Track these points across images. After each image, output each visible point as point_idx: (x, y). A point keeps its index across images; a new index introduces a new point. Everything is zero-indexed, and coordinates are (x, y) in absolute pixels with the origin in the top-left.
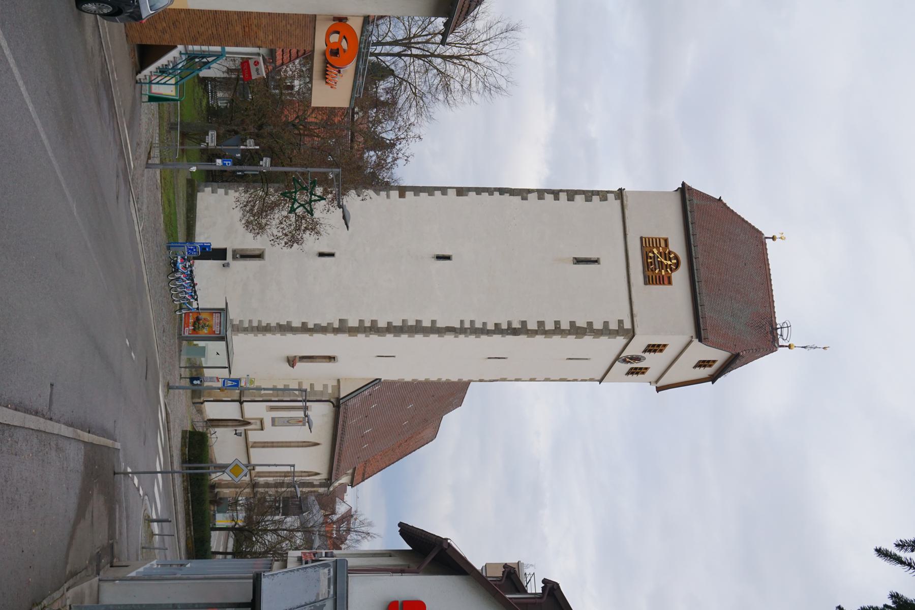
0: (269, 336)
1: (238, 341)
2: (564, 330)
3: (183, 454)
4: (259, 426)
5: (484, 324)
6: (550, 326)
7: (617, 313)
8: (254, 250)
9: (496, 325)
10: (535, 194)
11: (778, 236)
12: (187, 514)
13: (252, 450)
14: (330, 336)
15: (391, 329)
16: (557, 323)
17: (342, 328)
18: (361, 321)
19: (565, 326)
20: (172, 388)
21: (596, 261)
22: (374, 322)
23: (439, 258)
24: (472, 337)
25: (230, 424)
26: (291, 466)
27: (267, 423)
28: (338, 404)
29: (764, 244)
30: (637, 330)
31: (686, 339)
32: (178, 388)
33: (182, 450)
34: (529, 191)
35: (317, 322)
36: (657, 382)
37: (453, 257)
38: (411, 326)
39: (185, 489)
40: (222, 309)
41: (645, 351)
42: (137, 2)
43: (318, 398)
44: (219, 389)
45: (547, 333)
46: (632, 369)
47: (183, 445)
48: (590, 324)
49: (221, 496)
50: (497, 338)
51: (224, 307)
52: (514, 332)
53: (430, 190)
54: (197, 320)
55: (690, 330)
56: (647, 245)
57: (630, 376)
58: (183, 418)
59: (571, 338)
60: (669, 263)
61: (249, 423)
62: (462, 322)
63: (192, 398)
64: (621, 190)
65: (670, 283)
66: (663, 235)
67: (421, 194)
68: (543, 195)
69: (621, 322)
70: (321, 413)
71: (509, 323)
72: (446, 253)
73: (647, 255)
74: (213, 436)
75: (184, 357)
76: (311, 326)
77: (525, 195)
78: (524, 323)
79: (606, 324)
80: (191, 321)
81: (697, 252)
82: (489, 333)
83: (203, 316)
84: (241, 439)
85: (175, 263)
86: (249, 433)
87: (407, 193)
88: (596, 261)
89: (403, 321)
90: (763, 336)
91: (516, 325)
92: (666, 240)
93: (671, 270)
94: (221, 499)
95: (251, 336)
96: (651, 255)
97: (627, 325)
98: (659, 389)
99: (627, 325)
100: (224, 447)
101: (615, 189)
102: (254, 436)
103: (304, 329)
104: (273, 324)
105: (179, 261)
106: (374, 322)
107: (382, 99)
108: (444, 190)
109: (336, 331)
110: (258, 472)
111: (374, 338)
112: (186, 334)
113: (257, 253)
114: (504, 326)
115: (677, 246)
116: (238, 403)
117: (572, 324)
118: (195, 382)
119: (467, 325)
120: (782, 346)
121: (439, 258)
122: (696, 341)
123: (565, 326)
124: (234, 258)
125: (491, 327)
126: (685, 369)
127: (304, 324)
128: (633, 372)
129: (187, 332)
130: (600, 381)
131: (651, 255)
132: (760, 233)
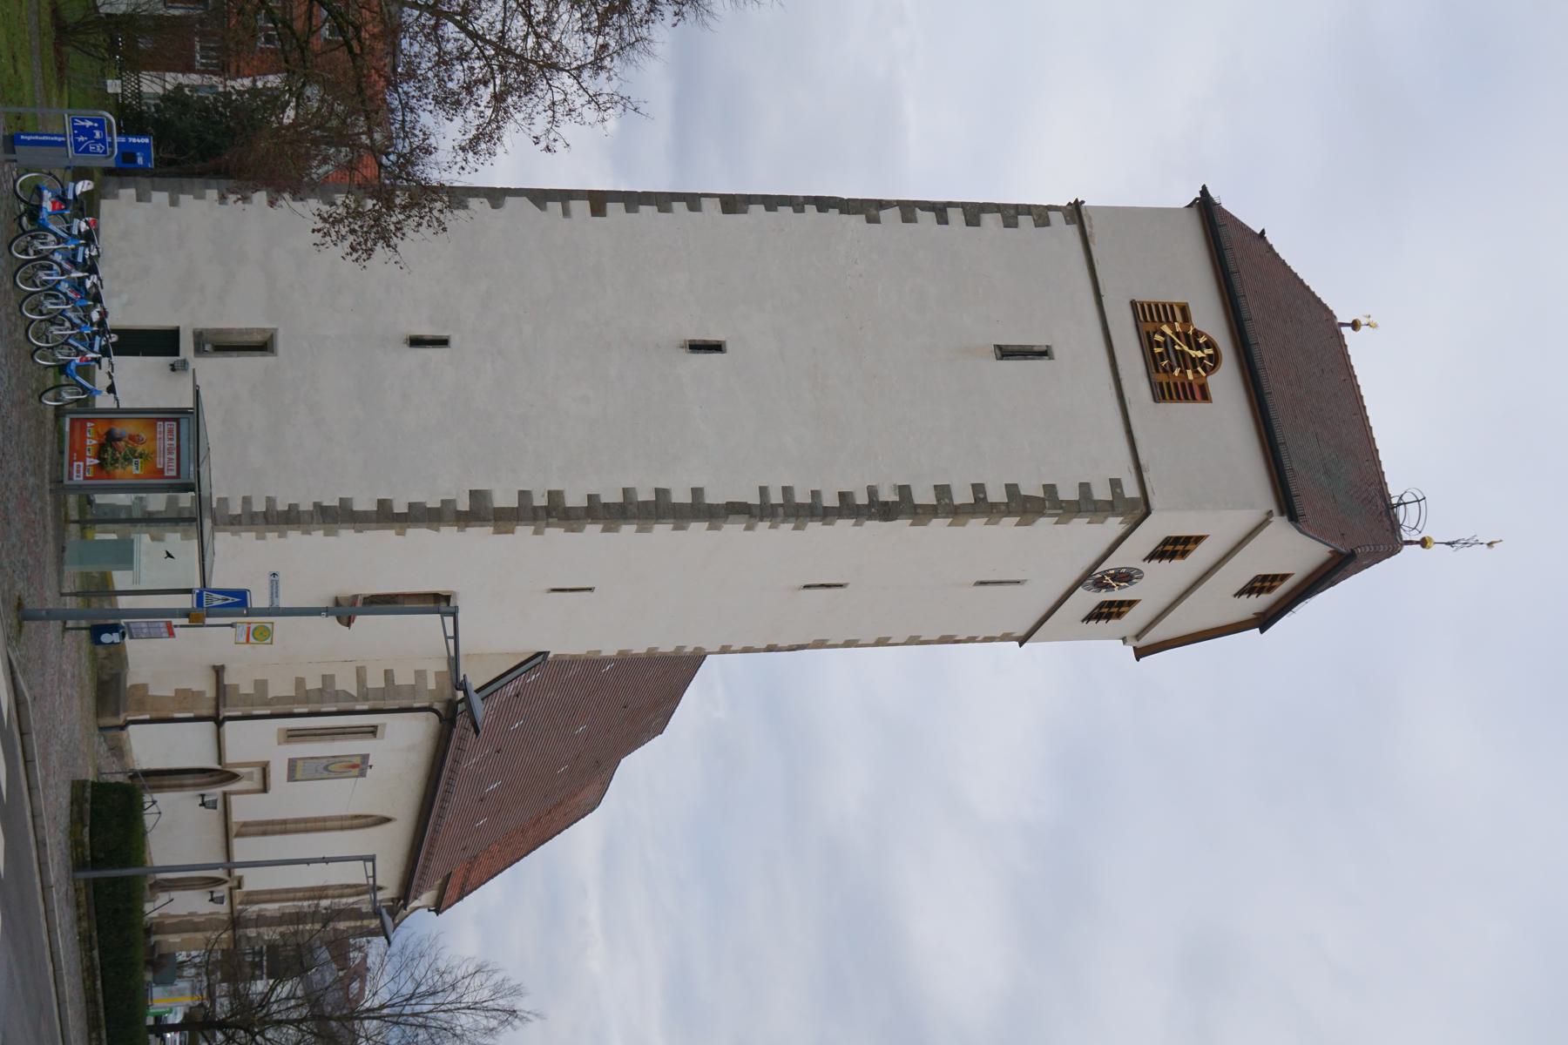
0: (294, 536)
2: (994, 505)
3: (76, 844)
4: (256, 784)
5: (816, 494)
6: (963, 496)
7: (1105, 465)
8: (249, 331)
9: (842, 496)
10: (896, 211)
11: (1363, 321)
12: (90, 1000)
14: (449, 533)
16: (978, 489)
17: (479, 512)
18: (524, 495)
19: (996, 495)
20: (33, 617)
21: (1044, 353)
22: (555, 496)
23: (697, 347)
25: (189, 780)
27: (278, 773)
28: (452, 716)
30: (1154, 501)
31: (1256, 516)
32: (50, 615)
33: (72, 833)
34: (882, 205)
36: (1138, 637)
37: (729, 347)
38: (645, 503)
39: (85, 940)
40: (183, 411)
41: (1152, 556)
42: (90, 1040)
43: (405, 703)
44: (186, 614)
45: (957, 513)
46: (1102, 605)
47: (76, 820)
48: (1050, 489)
49: (165, 950)
50: (844, 525)
51: (188, 403)
52: (885, 512)
54: (109, 440)
55: (1264, 499)
56: (1147, 315)
58: (70, 752)
60: (1200, 354)
61: (234, 777)
62: (763, 491)
63: (98, 715)
64: (1077, 205)
65: (1205, 397)
66: (1177, 298)
67: (642, 208)
68: (913, 212)
69: (1115, 484)
70: (403, 743)
71: (872, 492)
72: (713, 336)
73: (1149, 337)
74: (154, 809)
75: (71, 570)
76: (400, 507)
78: (904, 491)
79: (1085, 488)
80: (91, 442)
83: (125, 429)
84: (215, 816)
85: (34, 212)
86: (234, 799)
87: (609, 205)
88: (1044, 353)
89: (625, 491)
91: (888, 495)
92: (1184, 309)
93: (1204, 369)
94: (161, 956)
95: (248, 537)
96: (1158, 338)
97: (1131, 490)
98: (1140, 653)
99: (1131, 490)
100: (175, 831)
102: (245, 808)
103: (384, 516)
104: (306, 506)
105: (48, 205)
106: (555, 496)
108: (693, 201)
109: (465, 519)
110: (249, 894)
111: (555, 534)
112: (78, 479)
113: (258, 338)
114: (862, 499)
115: (1209, 319)
116: (211, 725)
117: (1012, 489)
118: (106, 638)
119: (776, 498)
121: (697, 347)
122: (1280, 524)
123: (996, 495)
124: (199, 350)
125: (831, 500)
126: (1220, 599)
127: (384, 504)
128: (1106, 612)
129: (80, 472)
130: (1022, 641)
131: (1158, 338)
132: (1330, 314)
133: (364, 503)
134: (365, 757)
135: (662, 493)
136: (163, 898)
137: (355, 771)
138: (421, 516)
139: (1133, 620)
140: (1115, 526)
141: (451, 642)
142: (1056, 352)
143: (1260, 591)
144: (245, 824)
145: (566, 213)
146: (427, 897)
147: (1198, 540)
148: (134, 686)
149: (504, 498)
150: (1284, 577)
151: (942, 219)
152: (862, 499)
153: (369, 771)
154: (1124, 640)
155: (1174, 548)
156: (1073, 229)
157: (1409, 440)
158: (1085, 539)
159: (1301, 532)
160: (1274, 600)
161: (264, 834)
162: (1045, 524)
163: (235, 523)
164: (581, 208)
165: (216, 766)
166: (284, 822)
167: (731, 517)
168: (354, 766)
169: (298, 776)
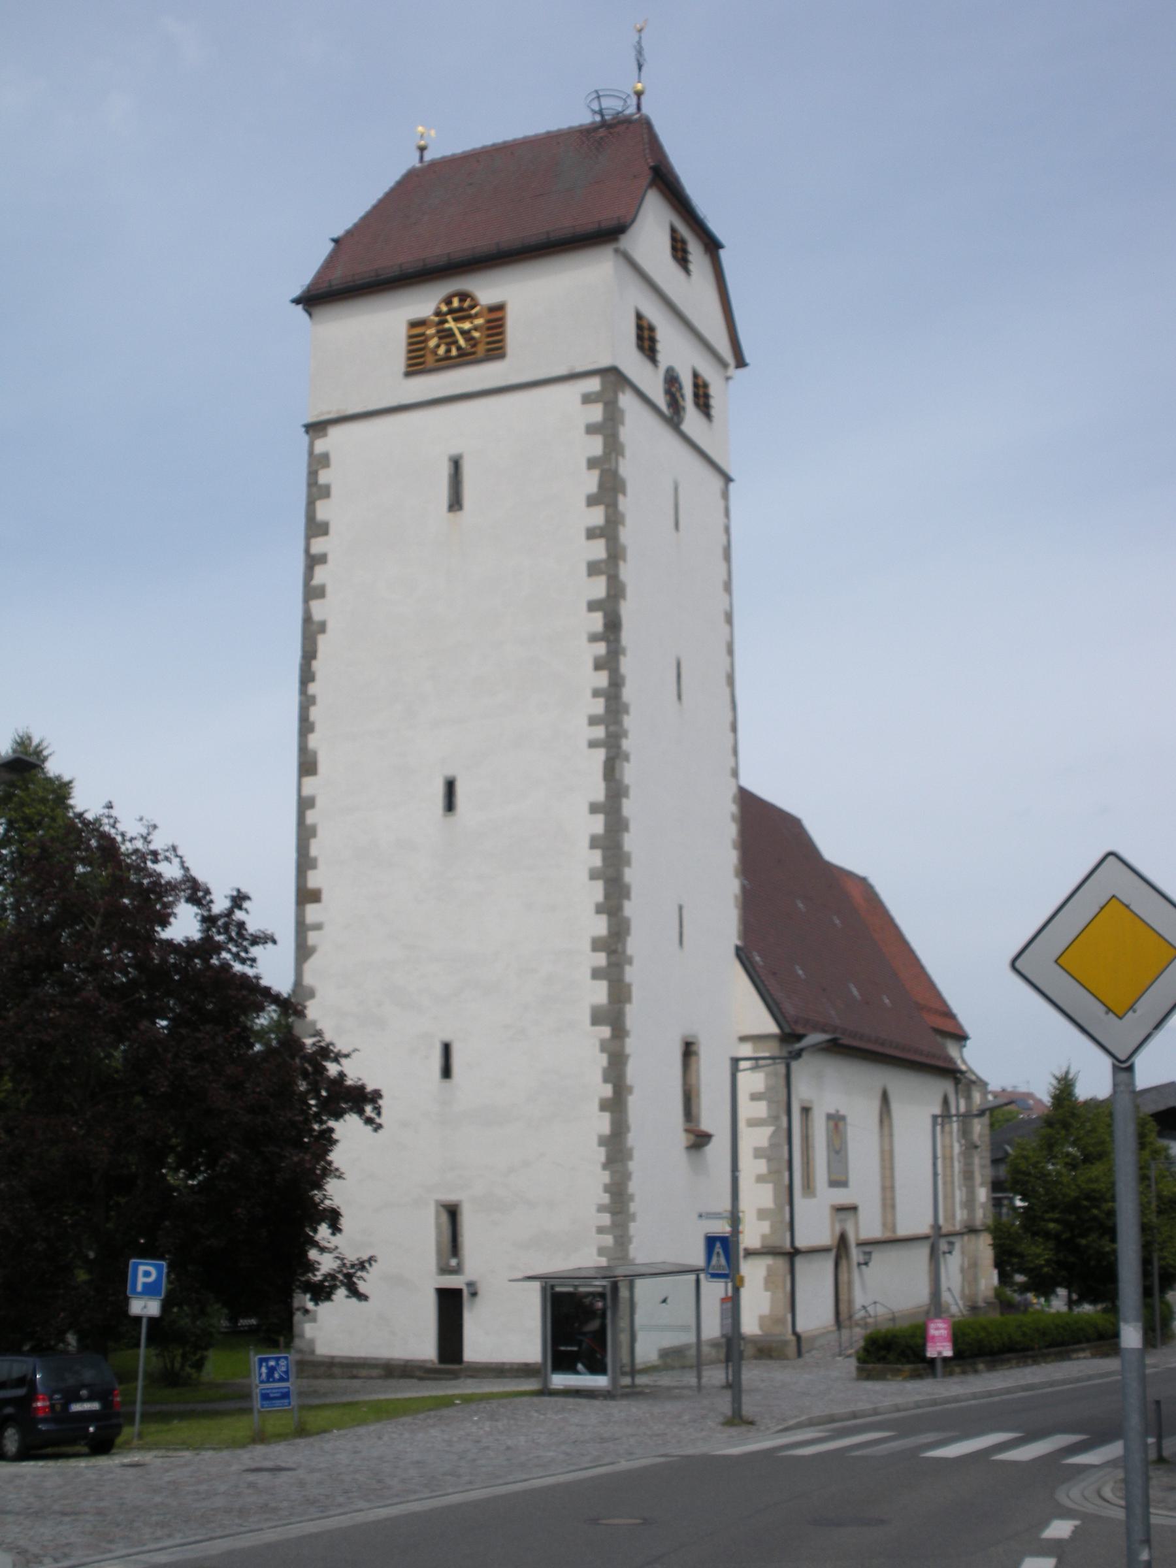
0: (633, 1187)
1: (641, 1252)
5: (596, 693)
6: (598, 550)
7: (569, 408)
10: (315, 605)
13: (902, 1232)
15: (614, 901)
16: (591, 534)
18: (596, 974)
23: (450, 805)
24: (628, 721)
27: (841, 1197)
29: (434, 164)
30: (604, 362)
34: (307, 619)
35: (598, 1076)
36: (724, 365)
38: (605, 859)
45: (615, 554)
46: (697, 404)
48: (592, 463)
50: (627, 665)
52: (613, 627)
53: (305, 834)
56: (419, 361)
57: (713, 412)
59: (625, 504)
61: (843, 1240)
62: (593, 744)
69: (587, 399)
71: (594, 638)
74: (871, 1309)
77: (314, 627)
79: (591, 429)
81: (437, 252)
82: (616, 682)
88: (456, 464)
92: (414, 324)
93: (473, 307)
96: (442, 351)
97: (593, 385)
98: (741, 363)
99: (593, 385)
100: (893, 1289)
101: (305, 439)
103: (616, 1105)
104: (605, 1177)
107: (275, 1016)
108: (305, 804)
109: (619, 1032)
110: (946, 1219)
111: (633, 945)
113: (445, 1218)
114: (601, 648)
115: (423, 303)
116: (800, 1262)
117: (592, 501)
119: (600, 732)
120: (639, 108)
121: (450, 805)
122: (625, 242)
123: (597, 516)
124: (457, 1271)
126: (694, 291)
127: (604, 1106)
128: (703, 401)
130: (728, 479)
133: (603, 1123)
134: (829, 1117)
135: (595, 842)
136: (946, 1297)
137: (841, 1124)
138: (616, 1070)
139: (709, 373)
140: (626, 400)
141: (761, 1062)
142: (454, 451)
143: (685, 251)
144: (884, 1225)
145: (318, 927)
146: (952, 1050)
147: (639, 317)
148: (761, 1327)
149: (599, 993)
150: (673, 231)
151: (322, 559)
152: (601, 648)
153: (842, 1112)
154: (728, 379)
155: (646, 341)
156: (334, 432)
157: (548, 105)
158: (640, 427)
159: (633, 221)
160: (695, 237)
161: (893, 1207)
162: (626, 468)
163: (622, 1240)
164: (312, 912)
165: (833, 1254)
166: (884, 1188)
167: (617, 776)
168: (836, 1126)
169: (843, 1178)
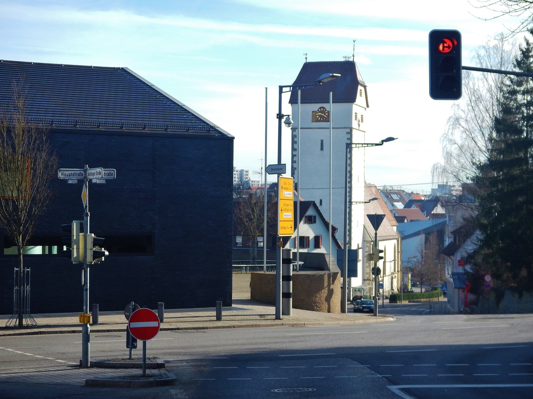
10: (294, 164)
26: (281, 92)
29: (309, 63)
69: (347, 133)
72: (319, 201)
90: (348, 68)
